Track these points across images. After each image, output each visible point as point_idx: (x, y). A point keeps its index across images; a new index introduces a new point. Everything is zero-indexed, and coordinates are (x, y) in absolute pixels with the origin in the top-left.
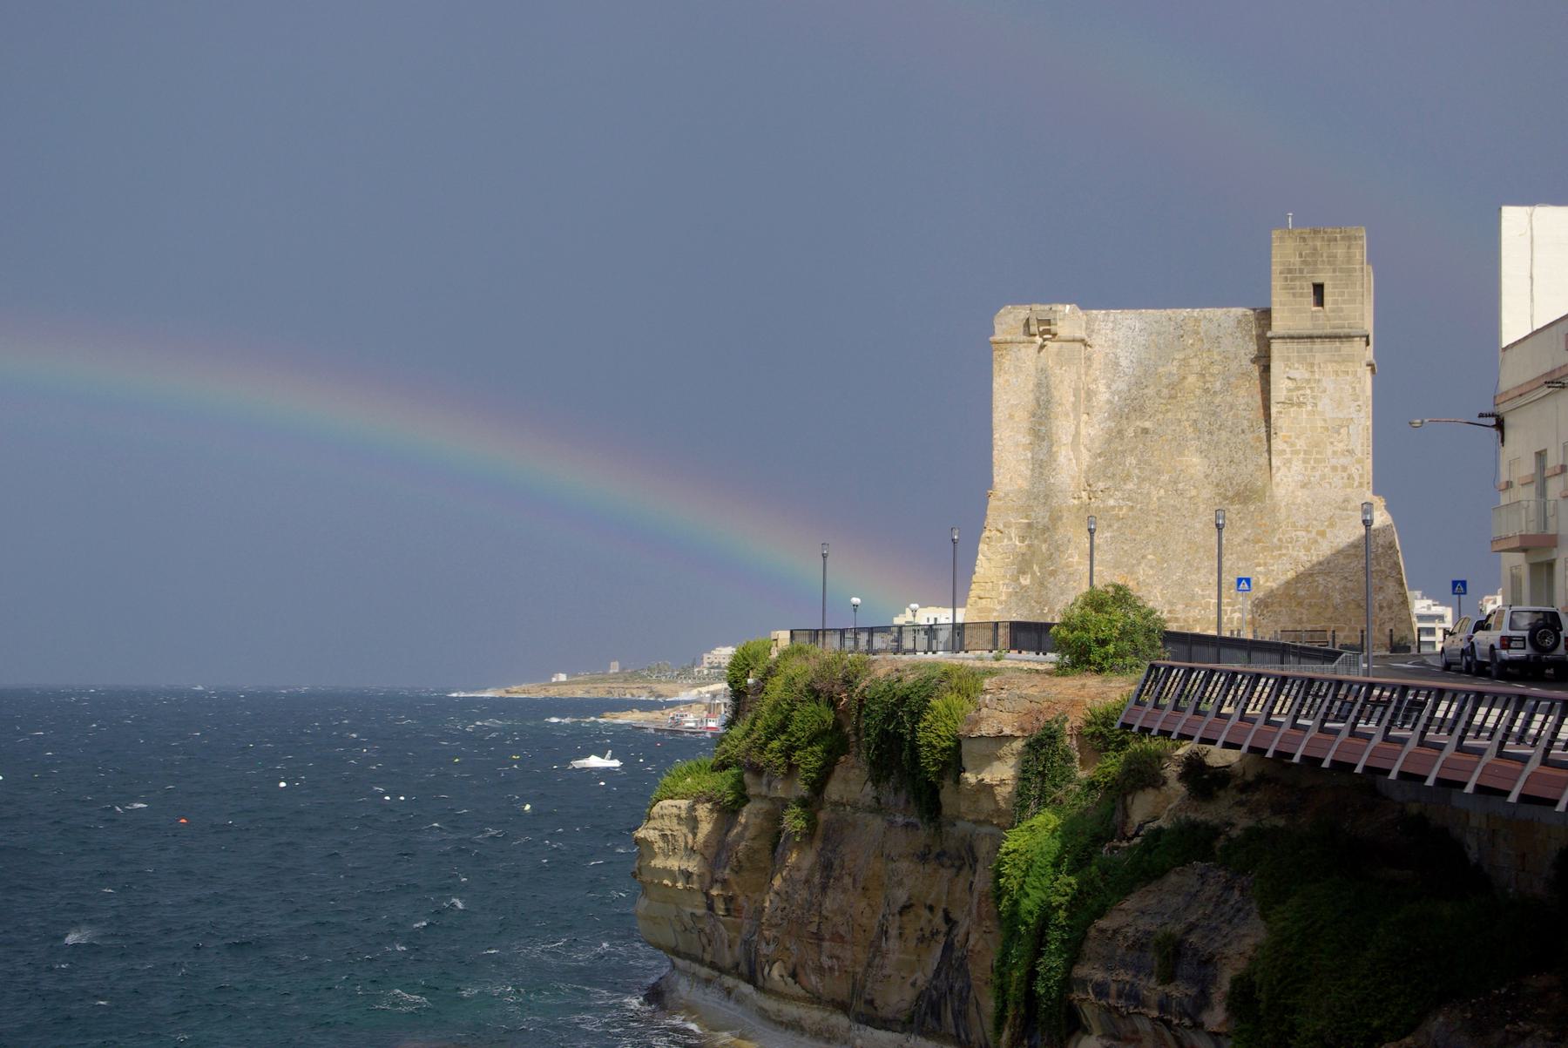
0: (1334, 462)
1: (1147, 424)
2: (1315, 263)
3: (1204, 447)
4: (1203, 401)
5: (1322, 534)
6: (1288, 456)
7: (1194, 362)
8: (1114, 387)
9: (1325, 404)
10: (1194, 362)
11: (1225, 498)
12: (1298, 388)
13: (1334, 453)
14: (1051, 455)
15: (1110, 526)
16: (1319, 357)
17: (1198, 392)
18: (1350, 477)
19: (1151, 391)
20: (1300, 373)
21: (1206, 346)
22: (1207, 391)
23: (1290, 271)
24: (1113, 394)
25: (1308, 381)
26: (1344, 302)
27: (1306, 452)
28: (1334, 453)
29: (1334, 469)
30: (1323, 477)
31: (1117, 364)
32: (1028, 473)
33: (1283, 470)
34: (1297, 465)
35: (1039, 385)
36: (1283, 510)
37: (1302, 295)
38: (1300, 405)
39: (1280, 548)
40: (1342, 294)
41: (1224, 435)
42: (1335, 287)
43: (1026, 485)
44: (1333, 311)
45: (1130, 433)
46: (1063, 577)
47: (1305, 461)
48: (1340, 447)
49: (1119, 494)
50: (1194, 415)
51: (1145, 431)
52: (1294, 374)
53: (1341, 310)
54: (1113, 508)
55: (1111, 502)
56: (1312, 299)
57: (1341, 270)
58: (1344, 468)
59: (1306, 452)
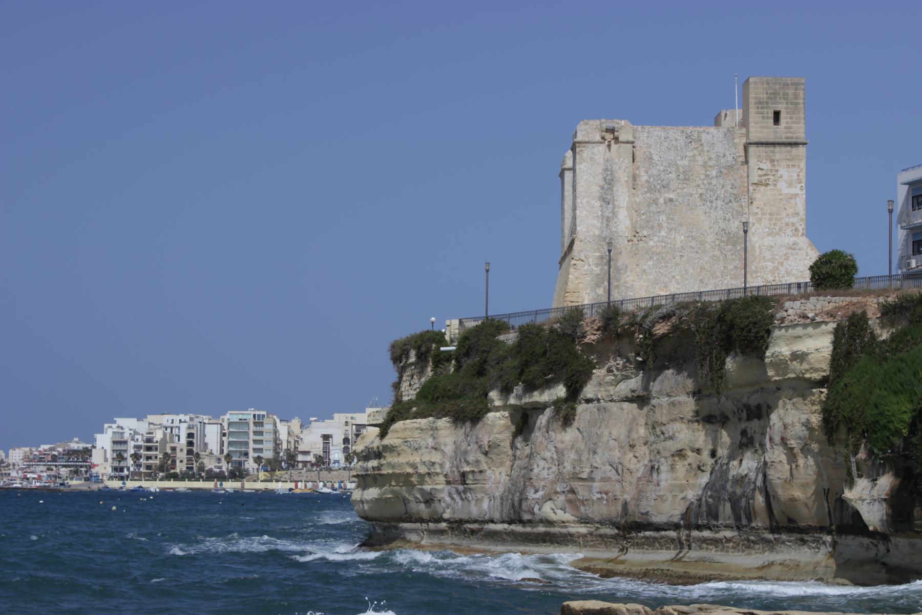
0: (787, 220)
1: (672, 196)
2: (775, 98)
3: (708, 210)
4: (705, 182)
5: (781, 264)
6: (760, 216)
7: (699, 158)
8: (650, 173)
9: (782, 185)
10: (699, 158)
11: (722, 241)
12: (766, 175)
13: (788, 215)
14: (614, 214)
15: (651, 258)
16: (778, 156)
17: (702, 177)
18: (796, 230)
19: (673, 176)
20: (766, 166)
21: (706, 149)
22: (707, 176)
23: (760, 103)
24: (650, 177)
25: (771, 170)
26: (793, 123)
27: (770, 214)
28: (788, 215)
29: (787, 224)
30: (781, 230)
31: (651, 158)
32: (599, 225)
33: (757, 225)
34: (765, 222)
35: (606, 170)
36: (757, 249)
37: (768, 118)
38: (767, 185)
39: (756, 272)
40: (791, 118)
41: (719, 203)
42: (788, 113)
43: (597, 232)
44: (786, 128)
45: (662, 201)
46: (623, 288)
47: (770, 219)
48: (791, 211)
49: (656, 239)
50: (700, 191)
51: (671, 200)
52: (762, 166)
53: (791, 128)
54: (653, 247)
55: (651, 243)
56: (772, 120)
57: (792, 103)
58: (793, 225)
59: (770, 214)
